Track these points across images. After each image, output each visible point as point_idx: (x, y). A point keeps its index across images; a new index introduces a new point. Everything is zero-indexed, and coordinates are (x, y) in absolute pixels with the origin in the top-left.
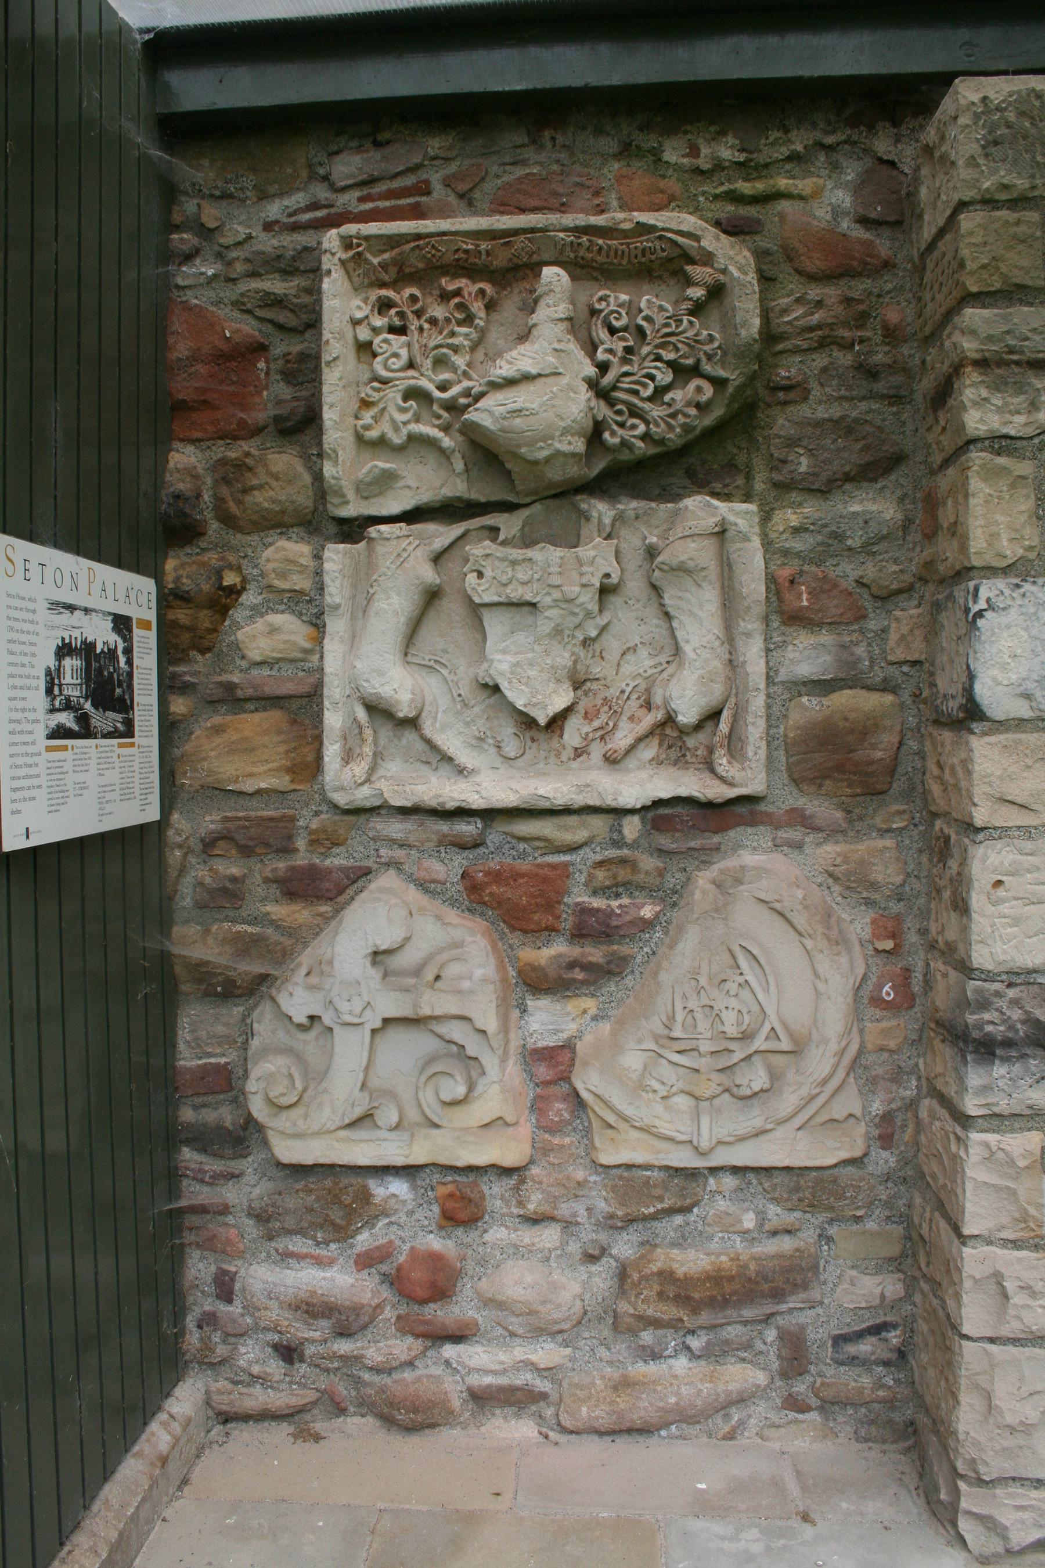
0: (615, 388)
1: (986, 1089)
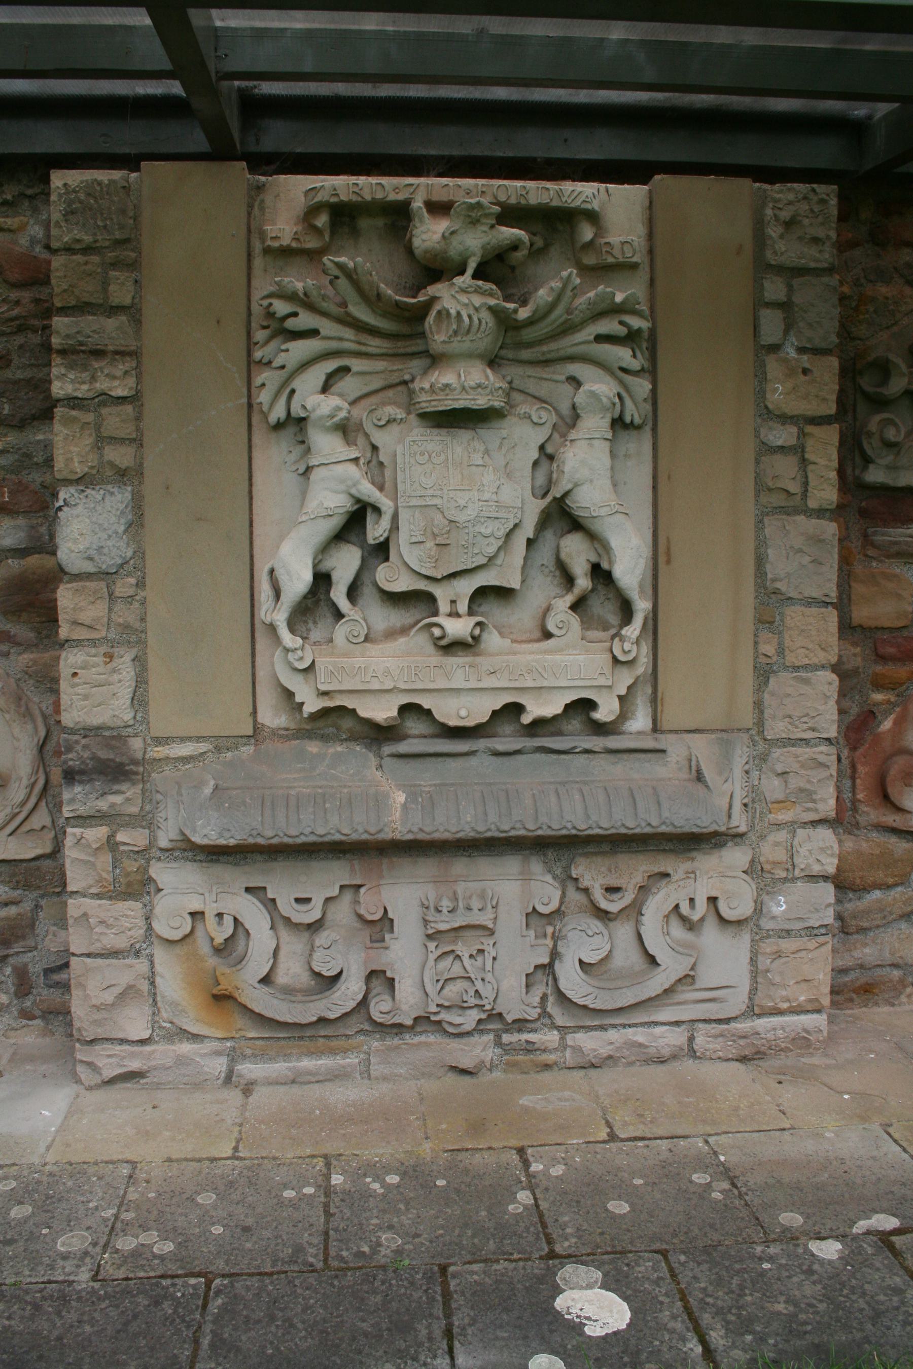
1: (72, 801)
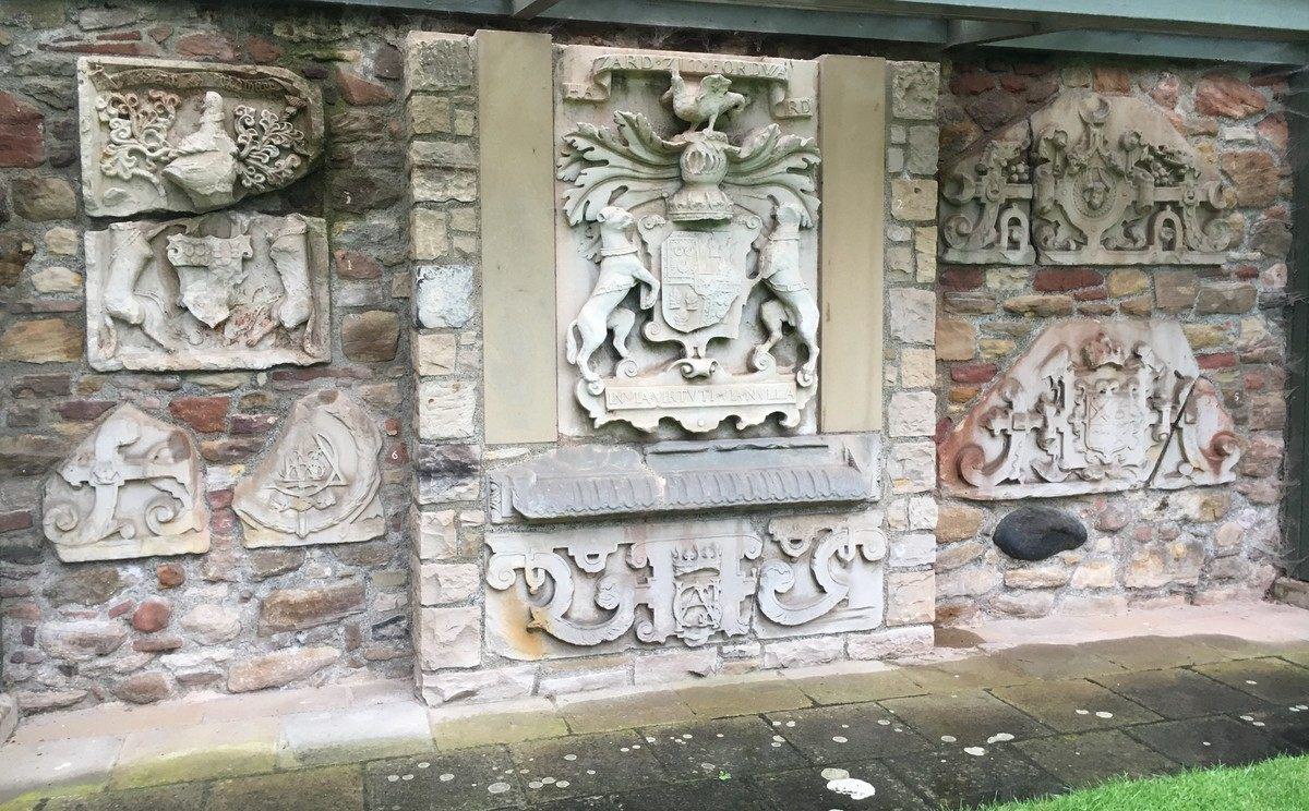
0: (248, 157)
1: (427, 492)
